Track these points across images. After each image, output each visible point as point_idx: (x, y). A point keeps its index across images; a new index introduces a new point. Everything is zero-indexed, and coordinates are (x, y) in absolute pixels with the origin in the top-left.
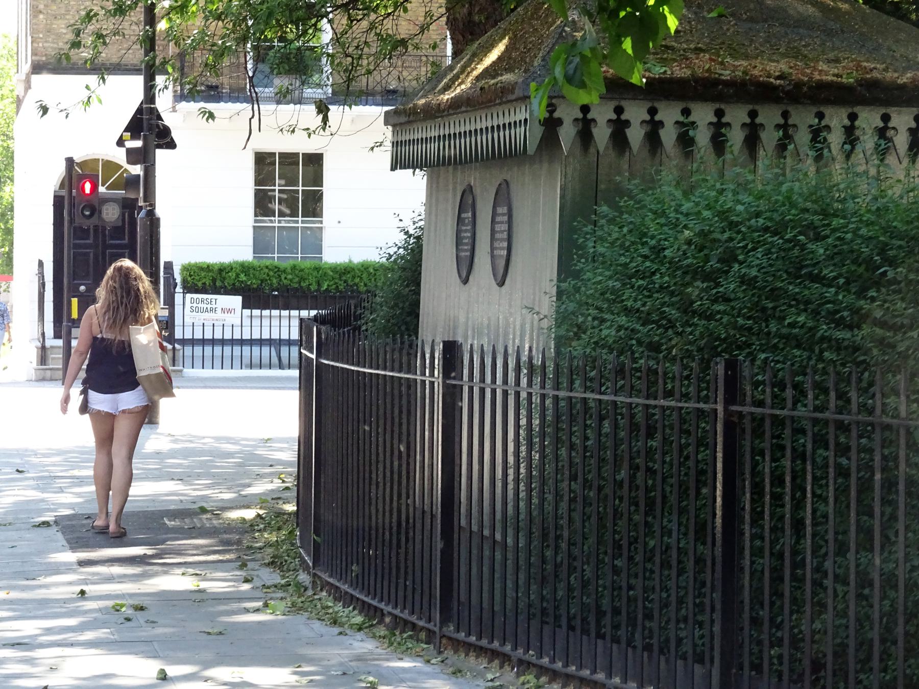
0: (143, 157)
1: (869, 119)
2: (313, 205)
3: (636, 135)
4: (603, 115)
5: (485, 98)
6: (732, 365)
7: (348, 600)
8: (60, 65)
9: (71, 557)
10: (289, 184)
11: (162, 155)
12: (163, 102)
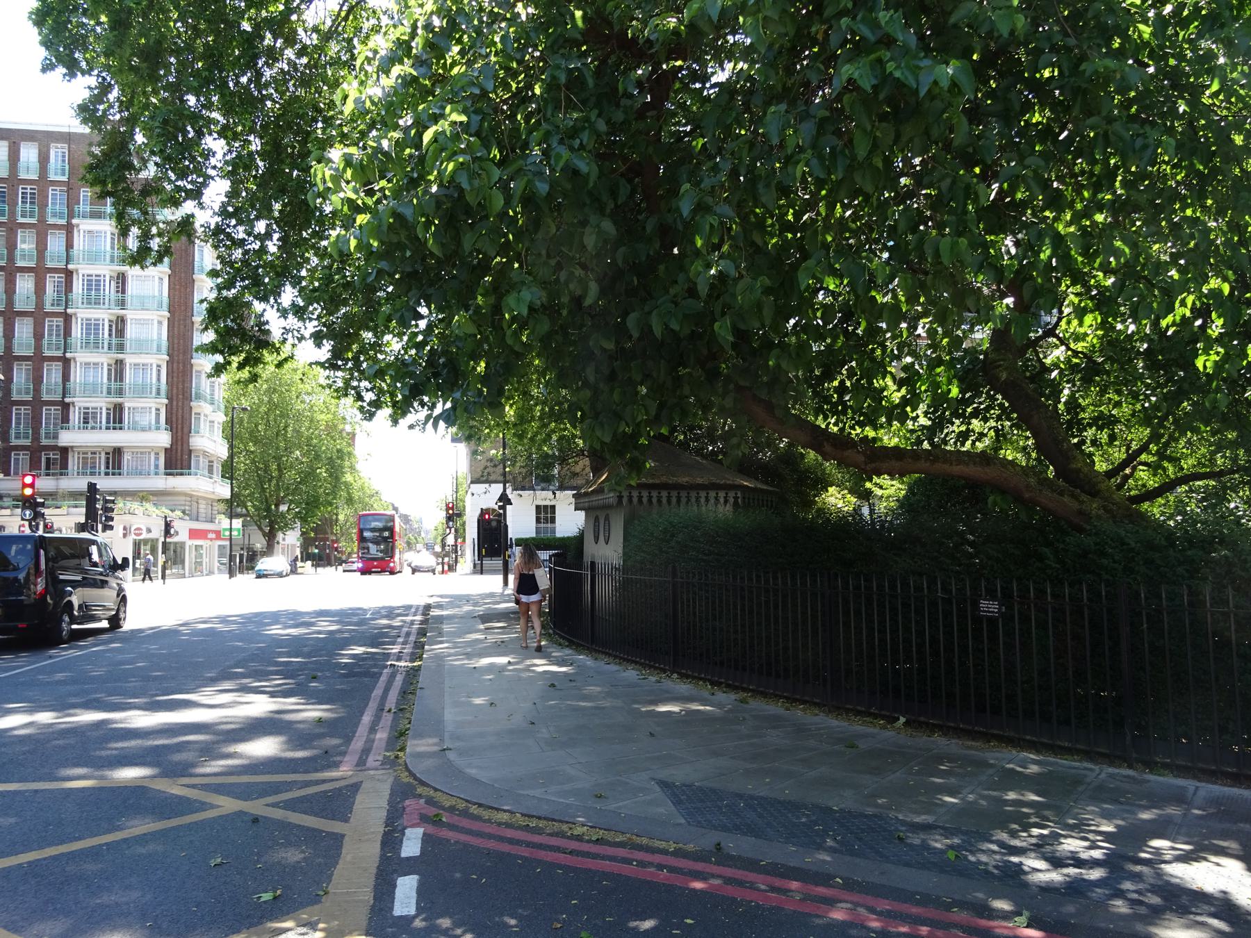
0: (503, 508)
1: (712, 494)
2: (553, 520)
3: (645, 500)
4: (625, 494)
5: (599, 491)
6: (674, 567)
7: (564, 638)
8: (475, 481)
9: (482, 627)
10: (546, 514)
11: (508, 507)
12: (509, 491)
